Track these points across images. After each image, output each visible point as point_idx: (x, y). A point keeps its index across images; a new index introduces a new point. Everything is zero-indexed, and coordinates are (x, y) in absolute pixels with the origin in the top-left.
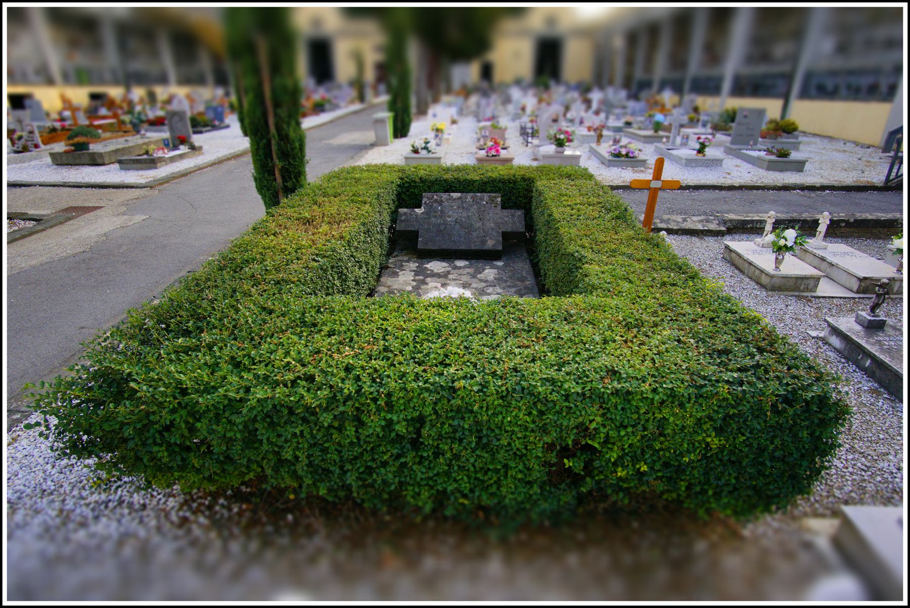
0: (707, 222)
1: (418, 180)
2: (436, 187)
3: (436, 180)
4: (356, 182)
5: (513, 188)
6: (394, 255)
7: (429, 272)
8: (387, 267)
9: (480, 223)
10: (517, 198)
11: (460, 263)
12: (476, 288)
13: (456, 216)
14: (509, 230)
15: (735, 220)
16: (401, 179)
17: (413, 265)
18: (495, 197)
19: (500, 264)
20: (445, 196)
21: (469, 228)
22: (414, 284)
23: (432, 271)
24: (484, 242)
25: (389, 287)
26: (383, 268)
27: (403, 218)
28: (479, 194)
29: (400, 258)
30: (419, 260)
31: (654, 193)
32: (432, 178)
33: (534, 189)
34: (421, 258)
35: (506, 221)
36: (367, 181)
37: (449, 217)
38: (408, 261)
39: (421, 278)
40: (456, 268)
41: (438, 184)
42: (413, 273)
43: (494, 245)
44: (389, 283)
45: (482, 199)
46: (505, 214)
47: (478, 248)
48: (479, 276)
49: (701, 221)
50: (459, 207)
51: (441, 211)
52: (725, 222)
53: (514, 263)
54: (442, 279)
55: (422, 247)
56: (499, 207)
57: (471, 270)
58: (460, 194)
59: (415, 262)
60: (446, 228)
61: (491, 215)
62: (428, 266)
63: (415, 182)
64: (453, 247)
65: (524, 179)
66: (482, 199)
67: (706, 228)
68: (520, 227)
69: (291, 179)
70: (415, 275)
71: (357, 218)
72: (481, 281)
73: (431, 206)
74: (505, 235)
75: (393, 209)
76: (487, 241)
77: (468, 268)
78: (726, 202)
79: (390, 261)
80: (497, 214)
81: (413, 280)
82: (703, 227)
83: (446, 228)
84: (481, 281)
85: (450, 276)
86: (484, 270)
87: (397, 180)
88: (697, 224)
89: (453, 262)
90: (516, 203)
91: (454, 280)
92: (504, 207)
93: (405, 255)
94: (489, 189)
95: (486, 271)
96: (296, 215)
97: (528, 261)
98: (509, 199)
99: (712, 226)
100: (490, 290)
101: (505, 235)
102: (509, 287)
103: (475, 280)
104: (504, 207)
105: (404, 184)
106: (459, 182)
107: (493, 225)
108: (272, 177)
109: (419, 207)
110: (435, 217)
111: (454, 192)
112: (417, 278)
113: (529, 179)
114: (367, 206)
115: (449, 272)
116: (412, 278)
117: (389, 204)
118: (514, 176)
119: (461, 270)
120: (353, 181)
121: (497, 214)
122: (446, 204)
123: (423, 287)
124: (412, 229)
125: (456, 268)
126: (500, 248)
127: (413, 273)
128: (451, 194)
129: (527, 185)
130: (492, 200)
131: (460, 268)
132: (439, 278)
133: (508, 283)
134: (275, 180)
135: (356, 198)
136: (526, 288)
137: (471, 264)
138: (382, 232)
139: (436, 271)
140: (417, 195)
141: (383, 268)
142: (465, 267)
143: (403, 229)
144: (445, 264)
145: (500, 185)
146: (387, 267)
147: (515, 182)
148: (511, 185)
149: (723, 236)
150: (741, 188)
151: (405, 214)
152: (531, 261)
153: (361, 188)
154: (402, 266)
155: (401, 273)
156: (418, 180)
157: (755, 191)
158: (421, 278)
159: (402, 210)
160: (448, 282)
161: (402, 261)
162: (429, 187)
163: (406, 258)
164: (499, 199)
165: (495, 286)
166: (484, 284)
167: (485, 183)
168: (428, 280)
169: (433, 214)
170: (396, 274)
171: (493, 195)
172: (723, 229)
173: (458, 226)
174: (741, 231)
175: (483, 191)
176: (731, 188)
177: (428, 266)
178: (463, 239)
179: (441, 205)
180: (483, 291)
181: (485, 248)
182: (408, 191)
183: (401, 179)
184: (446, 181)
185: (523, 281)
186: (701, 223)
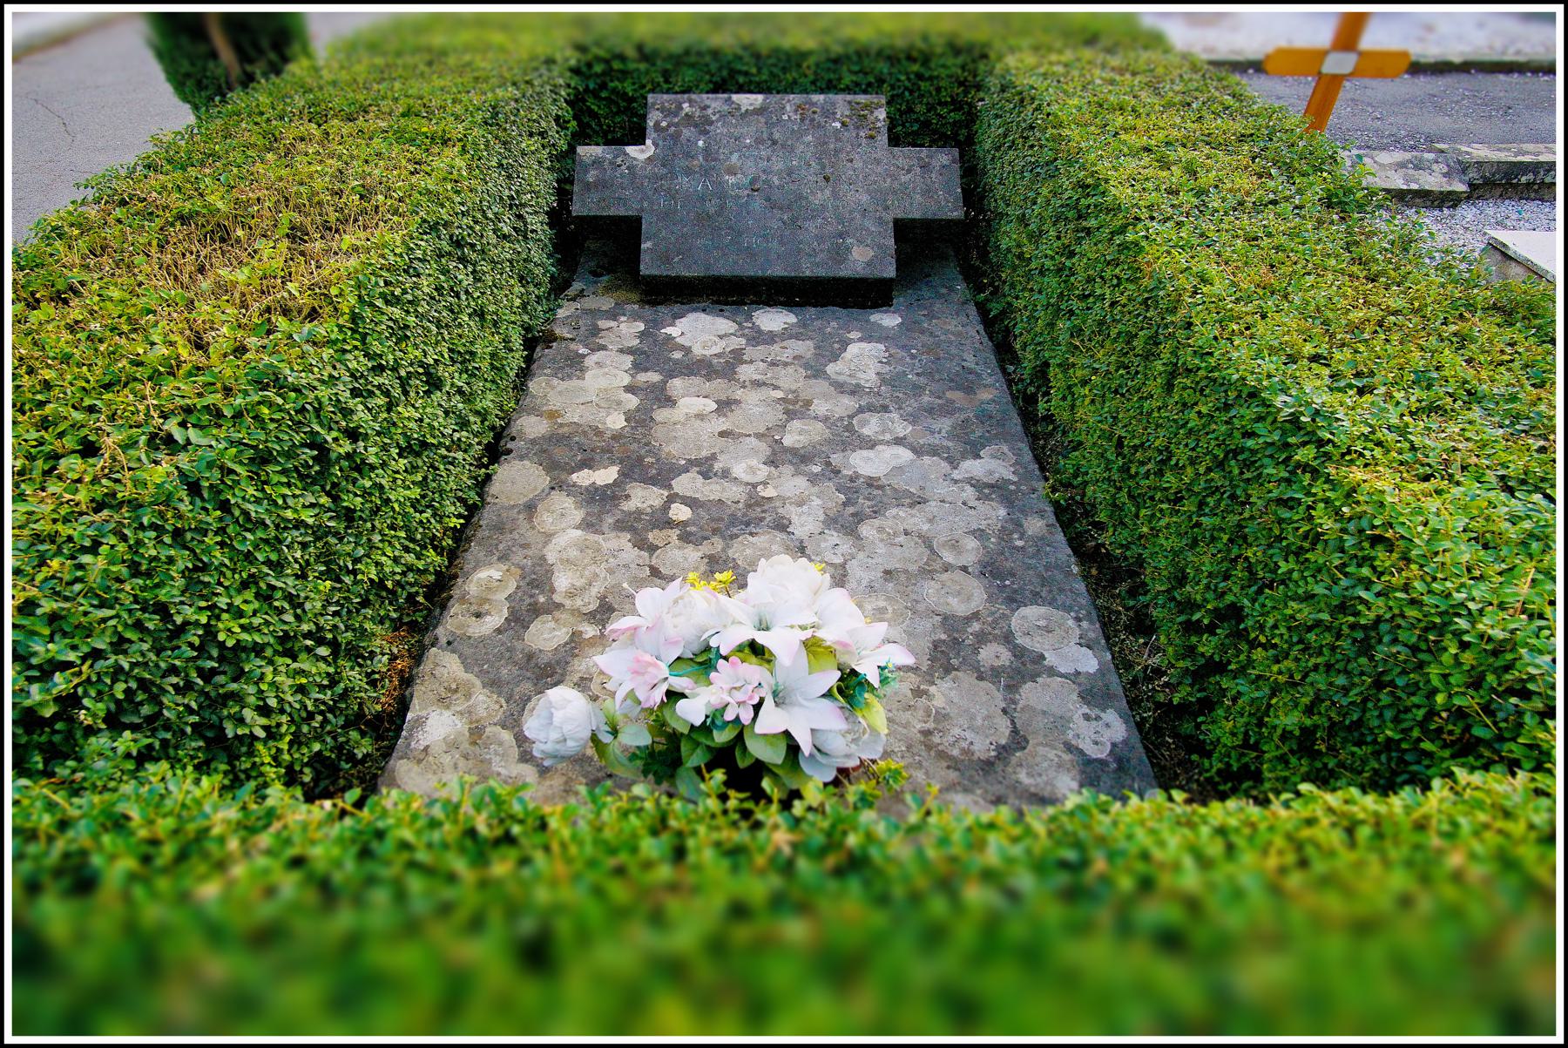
0: (1417, 168)
1: (631, 52)
2: (689, 75)
3: (687, 52)
4: (430, 64)
5: (920, 77)
6: (571, 292)
7: (677, 355)
8: (549, 339)
9: (827, 192)
10: (930, 108)
11: (773, 320)
12: (826, 420)
13: (751, 168)
14: (917, 215)
15: (1491, 163)
16: (582, 48)
17: (628, 329)
18: (870, 107)
19: (889, 320)
20: (715, 103)
21: (794, 208)
22: (632, 401)
23: (687, 350)
24: (840, 254)
25: (553, 415)
26: (535, 341)
27: (591, 176)
28: (819, 98)
29: (590, 302)
30: (648, 311)
31: (1328, 88)
32: (676, 47)
33: (993, 83)
34: (654, 303)
35: (904, 186)
36: (467, 58)
37: (732, 171)
38: (613, 315)
39: (654, 377)
40: (760, 338)
41: (693, 66)
42: (628, 360)
43: (868, 264)
44: (555, 402)
45: (829, 114)
46: (901, 162)
47: (821, 272)
48: (831, 369)
49: (1402, 165)
50: (759, 141)
51: (706, 150)
52: (1464, 168)
53: (931, 316)
54: (718, 383)
55: (655, 272)
56: (883, 139)
57: (805, 348)
58: (760, 97)
59: (635, 317)
60: (722, 207)
61: (858, 164)
62: (672, 331)
63: (622, 58)
64: (750, 270)
65: (955, 49)
66: (829, 114)
67: (1414, 187)
68: (950, 208)
69: (261, 52)
70: (638, 367)
71: (403, 208)
72: (840, 388)
73: (676, 137)
74: (904, 230)
75: (563, 145)
76: (849, 249)
77: (797, 337)
78: (1439, 109)
79: (561, 313)
80: (878, 162)
81: (630, 389)
82: (1407, 182)
83: (722, 207)
84: (840, 388)
85: (746, 372)
86: (845, 344)
87: (569, 52)
88: (1391, 173)
89: (749, 318)
90: (926, 124)
91: (757, 384)
92: (894, 141)
93: (608, 289)
94: (848, 79)
95: (853, 349)
96: (177, 202)
97: (972, 310)
98: (910, 110)
99: (1431, 179)
100: (871, 426)
101: (904, 230)
102: (930, 411)
103: (821, 386)
104: (894, 141)
105: (589, 65)
106: (757, 56)
107: (865, 198)
108: (202, 49)
109: (639, 139)
110: (688, 172)
111: (741, 89)
112: (643, 377)
113: (969, 48)
114: (452, 152)
115: (737, 357)
116: (627, 380)
117: (542, 134)
118: (925, 38)
119: (776, 347)
120: (419, 60)
121: (878, 162)
122: (719, 129)
123: (661, 415)
124: (622, 212)
125: (760, 338)
126: (890, 272)
127: (628, 360)
128: (735, 97)
129: (963, 68)
130: (860, 117)
131: (771, 338)
132: (708, 377)
133: (926, 399)
134: (214, 55)
135: (412, 124)
136: (984, 417)
137: (803, 324)
138: (523, 233)
139: (698, 351)
140: (632, 100)
141: (535, 341)
142: (787, 334)
143: (595, 212)
144: (724, 325)
145: (883, 67)
146: (549, 339)
147: (926, 59)
148: (915, 68)
149: (1454, 206)
150: (1466, 67)
151: (597, 162)
152: (982, 309)
153: (434, 87)
154: (595, 331)
155: (590, 361)
156: (631, 52)
157: (1502, 77)
158: (654, 377)
159: (586, 152)
160: (739, 394)
161: (595, 313)
162: (666, 75)
163: (607, 303)
164: (882, 114)
165: (885, 409)
166: (848, 404)
167: (837, 61)
168: (677, 385)
169: (682, 163)
170: (575, 365)
171: (862, 98)
172: (1461, 187)
173: (758, 203)
174: (1498, 191)
175: (830, 87)
176: (1442, 68)
177: (672, 331)
178: (775, 244)
179: (706, 132)
180: (849, 428)
181: (844, 272)
182: (603, 86)
183: (582, 48)
184: (715, 53)
185: (969, 390)
186: (1402, 172)
